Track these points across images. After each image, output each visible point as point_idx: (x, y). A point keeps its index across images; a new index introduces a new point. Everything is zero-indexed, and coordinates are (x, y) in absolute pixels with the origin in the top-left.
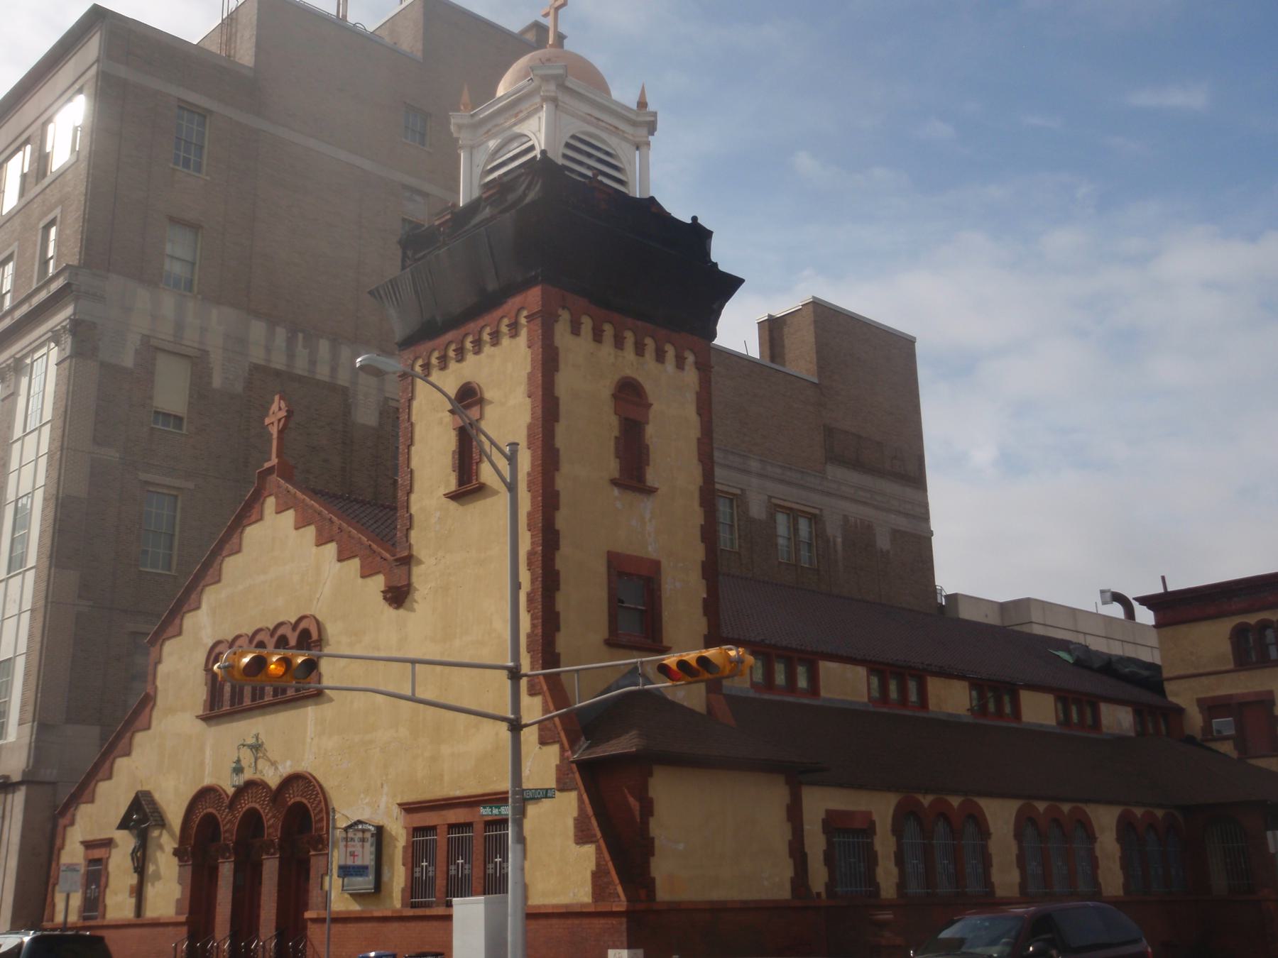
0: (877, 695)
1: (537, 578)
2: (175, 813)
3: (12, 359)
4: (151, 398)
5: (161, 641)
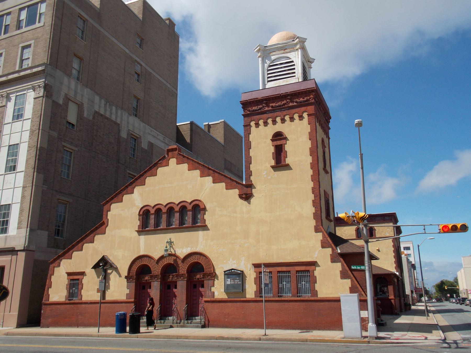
4: (67, 116)
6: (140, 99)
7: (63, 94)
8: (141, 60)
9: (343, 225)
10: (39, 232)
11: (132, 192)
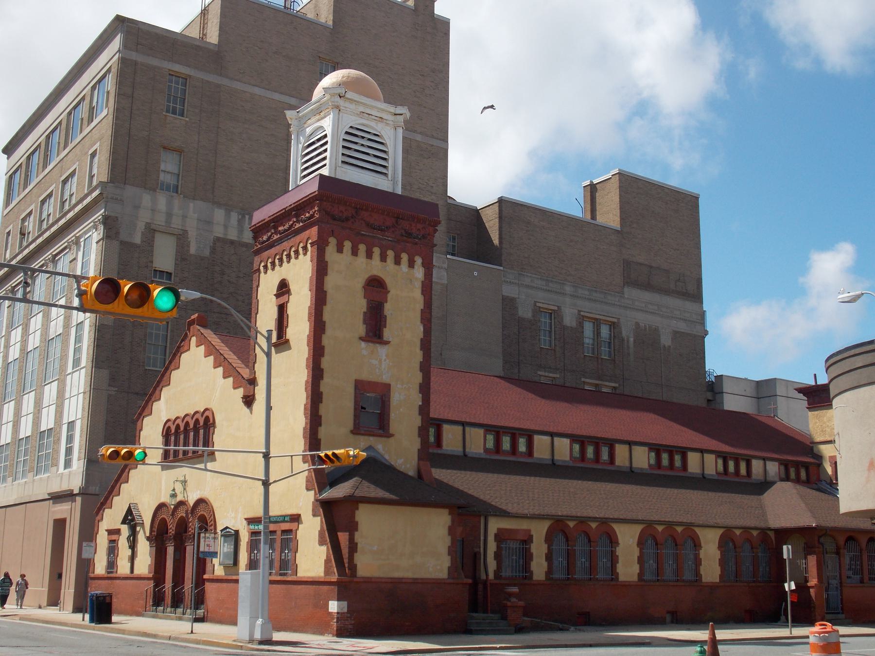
0: (578, 456)
1: (309, 396)
3: (74, 237)
4: (152, 262)
5: (142, 417)
7: (141, 226)
9: (824, 406)
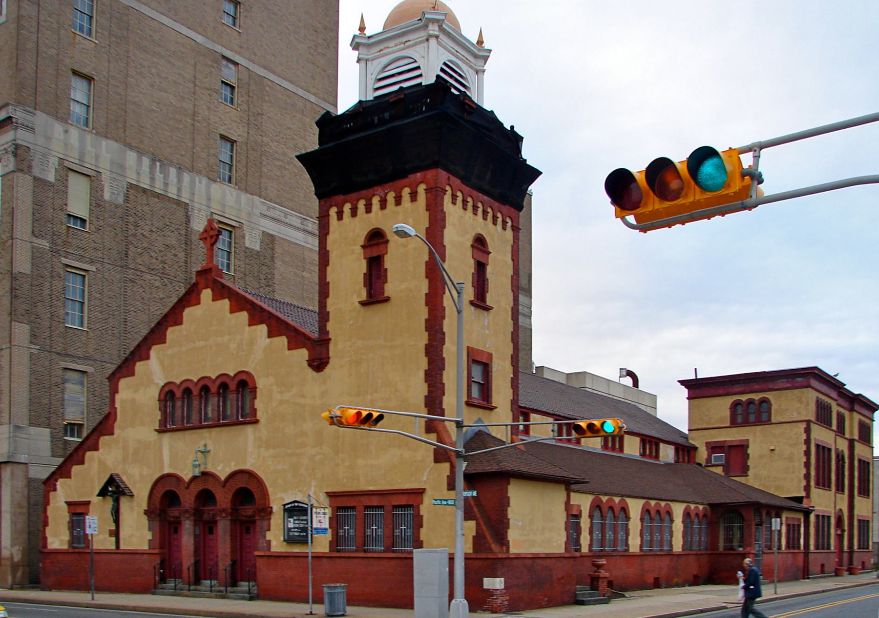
2: (141, 492)
4: (66, 205)
6: (236, 141)
7: (54, 162)
8: (236, 52)
10: (33, 430)
11: (148, 358)
